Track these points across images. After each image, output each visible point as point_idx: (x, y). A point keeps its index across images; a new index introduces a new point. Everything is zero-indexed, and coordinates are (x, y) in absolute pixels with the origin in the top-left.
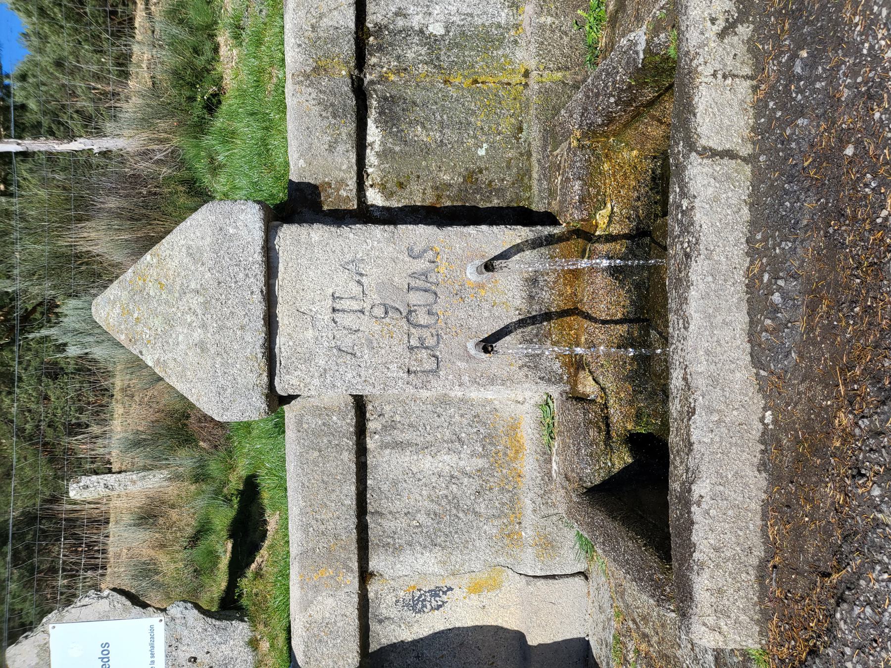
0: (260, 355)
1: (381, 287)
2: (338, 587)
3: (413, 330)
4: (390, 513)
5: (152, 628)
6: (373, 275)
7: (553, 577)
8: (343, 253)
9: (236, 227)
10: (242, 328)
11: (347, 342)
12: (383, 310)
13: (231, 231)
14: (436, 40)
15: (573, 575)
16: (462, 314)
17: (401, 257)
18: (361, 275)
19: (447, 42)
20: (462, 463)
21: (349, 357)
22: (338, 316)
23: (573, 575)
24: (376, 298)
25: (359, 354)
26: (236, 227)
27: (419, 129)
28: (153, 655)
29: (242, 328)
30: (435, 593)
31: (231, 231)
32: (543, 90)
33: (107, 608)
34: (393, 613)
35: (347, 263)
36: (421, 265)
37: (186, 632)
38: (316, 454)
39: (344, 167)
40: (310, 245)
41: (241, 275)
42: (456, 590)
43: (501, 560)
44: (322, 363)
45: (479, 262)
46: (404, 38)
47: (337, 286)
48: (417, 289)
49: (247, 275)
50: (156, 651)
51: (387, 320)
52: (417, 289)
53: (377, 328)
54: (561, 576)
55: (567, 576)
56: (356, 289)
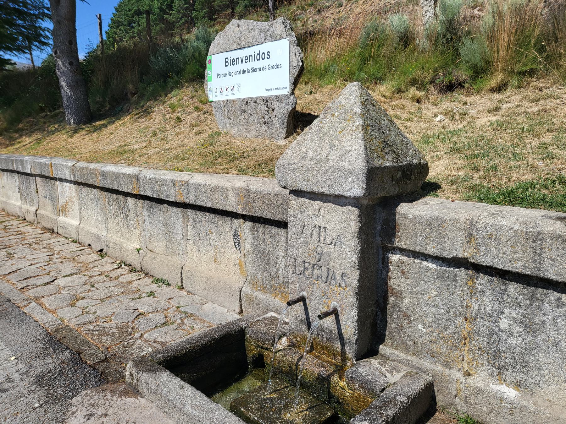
0: (297, 188)
1: (329, 254)
2: (238, 204)
3: (311, 265)
4: (265, 232)
5: (285, 88)
6: (334, 251)
7: (240, 299)
8: (344, 237)
9: (351, 183)
10: (308, 180)
11: (307, 231)
12: (320, 253)
13: (350, 179)
14: (496, 321)
15: (241, 308)
16: (317, 293)
17: (342, 268)
18: (335, 245)
19: (494, 328)
20: (281, 269)
21: (301, 231)
22: (317, 228)
23: (241, 308)
24: (325, 250)
25: (302, 235)
26: (351, 183)
27: (435, 293)
28: (276, 89)
29: (308, 180)
30: (239, 244)
31: (350, 179)
32: (451, 380)
33: (294, 65)
34: (233, 225)
35: (340, 239)
36: (339, 279)
37: (283, 105)
38: (281, 202)
39: (408, 242)
40: (348, 220)
41: (329, 183)
42: (240, 255)
43: (249, 277)
44: (299, 216)
45: (339, 309)
46: (498, 299)
47: (330, 231)
48: (328, 273)
49: (329, 186)
50: (280, 90)
51: (315, 254)
52: (328, 273)
53: (312, 248)
54: (241, 302)
55: (241, 305)
56: (328, 240)
